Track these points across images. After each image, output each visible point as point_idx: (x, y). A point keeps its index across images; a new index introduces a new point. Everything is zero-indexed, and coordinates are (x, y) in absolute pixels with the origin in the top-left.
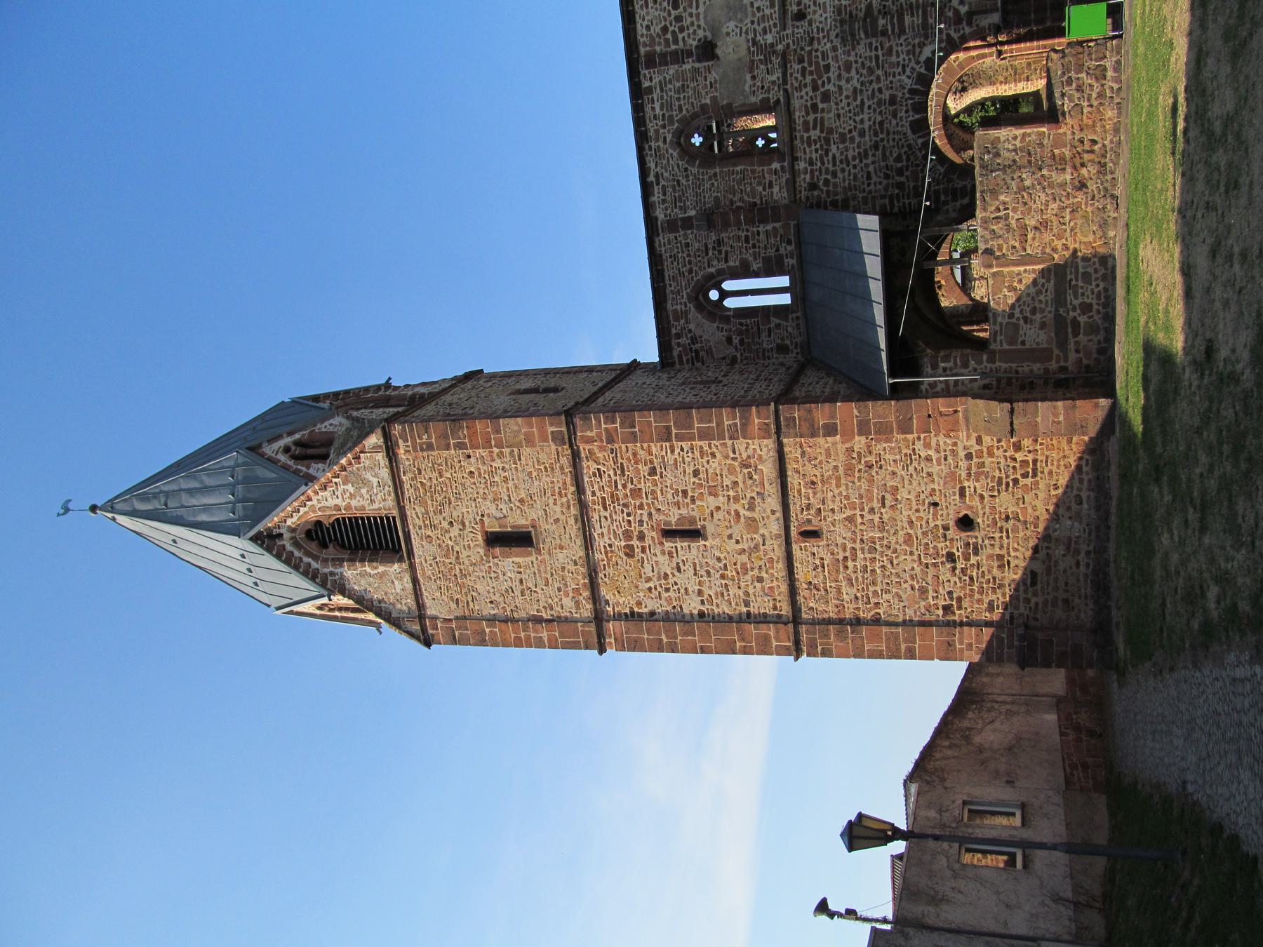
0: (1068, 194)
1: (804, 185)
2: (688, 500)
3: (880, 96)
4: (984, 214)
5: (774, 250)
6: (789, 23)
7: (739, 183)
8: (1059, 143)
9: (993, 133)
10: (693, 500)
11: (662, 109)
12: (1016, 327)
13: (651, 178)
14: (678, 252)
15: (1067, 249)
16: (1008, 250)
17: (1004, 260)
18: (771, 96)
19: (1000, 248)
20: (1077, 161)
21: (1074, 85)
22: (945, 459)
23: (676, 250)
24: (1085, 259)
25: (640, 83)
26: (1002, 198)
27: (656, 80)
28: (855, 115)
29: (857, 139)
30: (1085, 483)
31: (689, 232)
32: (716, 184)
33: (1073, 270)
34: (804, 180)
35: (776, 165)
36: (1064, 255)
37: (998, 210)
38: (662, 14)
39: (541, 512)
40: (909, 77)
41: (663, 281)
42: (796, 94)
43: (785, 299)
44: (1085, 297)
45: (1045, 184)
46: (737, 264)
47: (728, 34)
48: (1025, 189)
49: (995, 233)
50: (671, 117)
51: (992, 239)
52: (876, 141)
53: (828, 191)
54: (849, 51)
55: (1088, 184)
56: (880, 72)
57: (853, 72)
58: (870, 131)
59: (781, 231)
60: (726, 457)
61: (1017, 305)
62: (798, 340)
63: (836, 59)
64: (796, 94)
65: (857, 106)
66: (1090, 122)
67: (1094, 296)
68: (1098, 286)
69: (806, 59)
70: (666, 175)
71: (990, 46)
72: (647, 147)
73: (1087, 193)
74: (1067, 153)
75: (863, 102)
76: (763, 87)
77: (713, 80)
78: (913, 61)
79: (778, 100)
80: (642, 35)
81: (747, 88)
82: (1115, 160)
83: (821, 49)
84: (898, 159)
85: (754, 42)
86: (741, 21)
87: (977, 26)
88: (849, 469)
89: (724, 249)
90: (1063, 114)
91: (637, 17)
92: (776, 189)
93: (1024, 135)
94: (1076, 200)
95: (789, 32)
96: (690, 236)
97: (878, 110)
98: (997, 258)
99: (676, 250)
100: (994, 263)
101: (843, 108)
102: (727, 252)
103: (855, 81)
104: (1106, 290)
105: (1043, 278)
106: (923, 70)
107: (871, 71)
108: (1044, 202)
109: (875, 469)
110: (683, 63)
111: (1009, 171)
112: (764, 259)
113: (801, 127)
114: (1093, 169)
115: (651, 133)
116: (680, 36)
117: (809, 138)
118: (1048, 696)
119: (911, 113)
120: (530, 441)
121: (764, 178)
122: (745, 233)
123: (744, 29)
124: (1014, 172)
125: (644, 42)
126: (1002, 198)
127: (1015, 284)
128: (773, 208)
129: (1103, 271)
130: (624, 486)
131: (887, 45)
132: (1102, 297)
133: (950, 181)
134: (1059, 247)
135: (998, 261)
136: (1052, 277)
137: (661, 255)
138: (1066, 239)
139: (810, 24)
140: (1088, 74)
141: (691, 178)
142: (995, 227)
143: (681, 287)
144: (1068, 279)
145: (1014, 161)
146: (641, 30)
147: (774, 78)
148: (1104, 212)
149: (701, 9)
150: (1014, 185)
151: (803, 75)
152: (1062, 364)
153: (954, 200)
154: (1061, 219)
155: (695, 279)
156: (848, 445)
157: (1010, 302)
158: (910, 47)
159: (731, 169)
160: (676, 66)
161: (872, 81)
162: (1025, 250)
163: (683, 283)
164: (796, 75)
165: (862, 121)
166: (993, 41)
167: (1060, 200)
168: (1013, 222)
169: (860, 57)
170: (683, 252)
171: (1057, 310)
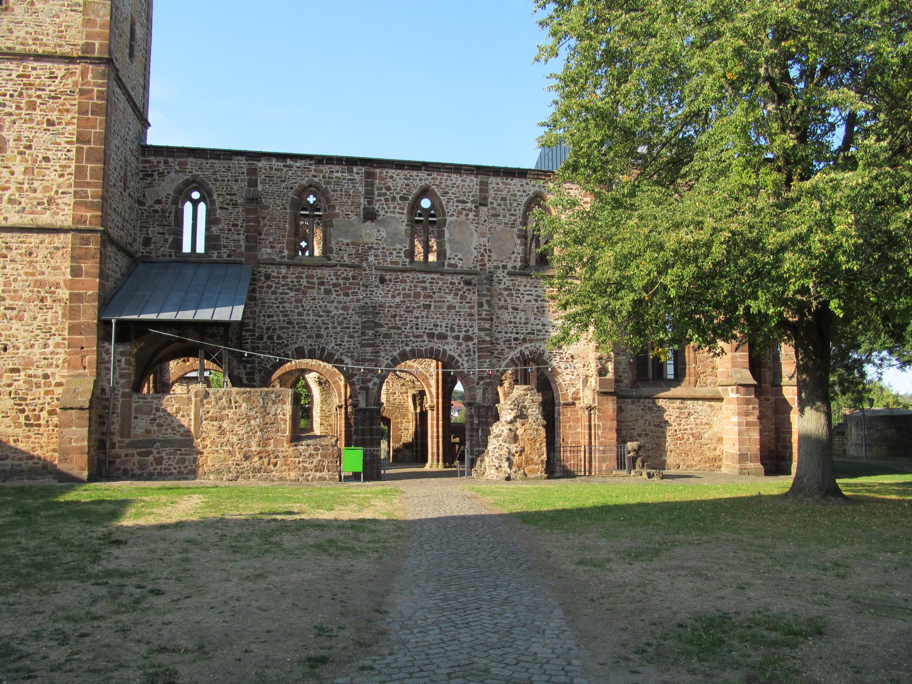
2: (22, 149)
6: (379, 273)
7: (277, 225)
8: (278, 442)
9: (289, 400)
10: (21, 153)
11: (336, 177)
12: (149, 413)
13: (289, 162)
19: (208, 403)
20: (264, 454)
22: (45, 359)
24: (195, 460)
25: (356, 165)
26: (244, 405)
27: (356, 177)
29: (296, 311)
30: (19, 462)
34: (273, 271)
35: (286, 252)
37: (236, 402)
39: (20, 18)
41: (211, 158)
43: (187, 248)
45: (251, 433)
47: (379, 231)
48: (249, 421)
50: (330, 183)
53: (263, 287)
56: (339, 329)
57: (342, 312)
59: (238, 251)
60: (59, 186)
62: (153, 255)
66: (289, 462)
68: (175, 468)
70: (290, 173)
71: (346, 401)
75: (321, 316)
79: (330, 260)
81: (342, 239)
84: (279, 337)
85: (370, 248)
86: (386, 241)
88: (41, 284)
89: (230, 207)
90: (296, 445)
92: (269, 251)
93: (285, 420)
95: (374, 272)
98: (202, 401)
102: (227, 209)
104: (171, 474)
106: (336, 357)
107: (340, 323)
109: (40, 304)
112: (219, 236)
115: (321, 167)
116: (382, 198)
117: (302, 278)
120: (87, 23)
124: (261, 413)
130: (39, 97)
133: (260, 371)
134: (205, 443)
139: (376, 286)
146: (391, 172)
147: (346, 258)
149: (397, 215)
150: (252, 413)
151: (344, 278)
152: (117, 445)
153: (247, 374)
156: (62, 284)
157: (169, 409)
165: (308, 315)
166: (348, 403)
168: (226, 412)
171: (159, 441)
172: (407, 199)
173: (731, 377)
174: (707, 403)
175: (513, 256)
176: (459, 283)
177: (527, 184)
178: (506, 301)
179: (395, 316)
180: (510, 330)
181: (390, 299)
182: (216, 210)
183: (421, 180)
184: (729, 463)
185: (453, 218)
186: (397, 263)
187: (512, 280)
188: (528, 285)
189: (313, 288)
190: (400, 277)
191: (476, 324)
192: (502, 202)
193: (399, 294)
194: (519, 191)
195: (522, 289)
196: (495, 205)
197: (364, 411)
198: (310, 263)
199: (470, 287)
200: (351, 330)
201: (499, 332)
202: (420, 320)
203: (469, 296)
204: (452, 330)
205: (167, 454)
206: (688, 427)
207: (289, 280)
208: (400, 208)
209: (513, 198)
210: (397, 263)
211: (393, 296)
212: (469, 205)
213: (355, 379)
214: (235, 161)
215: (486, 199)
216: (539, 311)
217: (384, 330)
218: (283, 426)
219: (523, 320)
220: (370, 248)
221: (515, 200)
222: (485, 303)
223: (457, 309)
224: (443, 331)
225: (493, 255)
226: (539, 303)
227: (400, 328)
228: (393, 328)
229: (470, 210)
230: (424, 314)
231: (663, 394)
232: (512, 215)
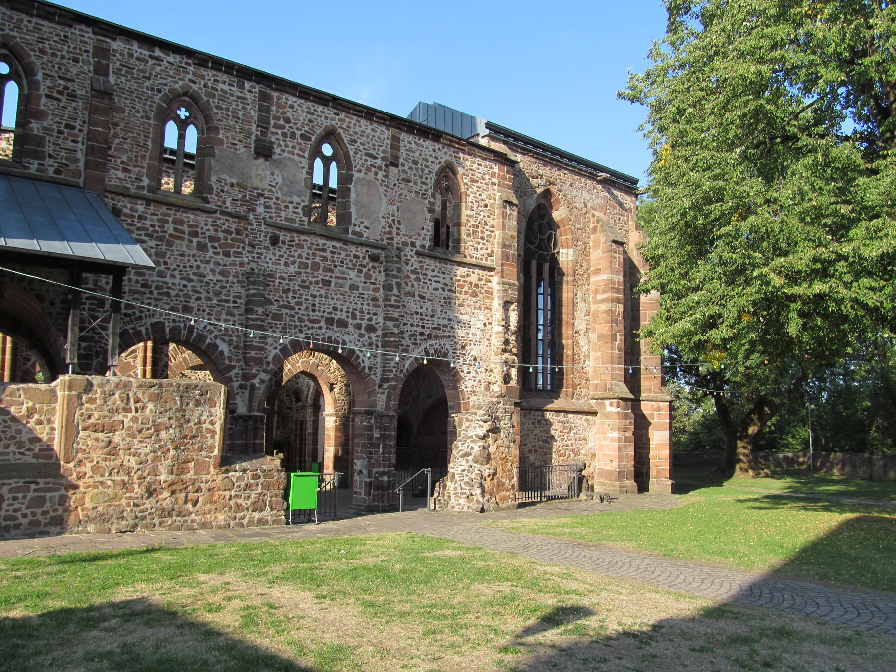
0: (145, 478)
1: (119, 205)
3: (193, 298)
4: (135, 385)
5: (51, 152)
6: (270, 230)
8: (201, 467)
9: (221, 400)
11: (222, 90)
13: (158, 53)
14: (69, 47)
15: (79, 478)
16: (87, 410)
17: (76, 404)
18: (213, 196)
19: (91, 401)
20: (178, 487)
21: (252, 481)
23: (72, 46)
24: (64, 499)
25: (250, 80)
26: (151, 406)
27: (248, 95)
28: (181, 271)
31: (91, 68)
32: (139, 115)
33: (50, 485)
35: (146, 182)
36: (71, 475)
37: (137, 401)
38: (300, 123)
40: (205, 327)
41: (38, 16)
42: (210, 220)
44: (11, 501)
45: (159, 453)
46: (42, 107)
47: (273, 174)
48: (158, 431)
49: (110, 395)
50: (213, 96)
51: (103, 392)
52: (151, 287)
54: (238, 277)
55: (151, 499)
56: (215, 301)
57: (219, 277)
58: (162, 282)
59: (72, 167)
61: (7, 418)
63: (234, 264)
64: (210, 220)
65: (188, 274)
66: (215, 498)
67: (11, 513)
68: (25, 516)
69: (238, 237)
70: (158, 68)
72: (190, 61)
73: (142, 498)
74: (189, 476)
75: (190, 280)
76: (222, 191)
77: (238, 147)
78: (218, 333)
79: (208, 202)
80: (287, 99)
81: (225, 176)
82: (174, 525)
83: (244, 252)
85: (261, 195)
86: (281, 189)
87: (238, 393)
90: (227, 471)
91: (303, 101)
92: (121, 174)
93: (214, 432)
94: (136, 486)
95: (263, 228)
96: (86, 67)
97: (181, 294)
98: (79, 397)
99: (72, 46)
100: (74, 392)
101: (189, 261)
102: (58, 100)
103: (211, 277)
104: (17, 526)
105: (41, 450)
106: (208, 341)
107: (217, 294)
108: (140, 451)
110: (258, 126)
111: (179, 414)
112: (43, 138)
113: (178, 216)
114: (168, 504)
115: (203, 71)
116: (280, 132)
117: (167, 222)
118: (301, 444)
119: (172, 324)
121: (135, 166)
122: (78, 127)
123: (273, 189)
124: (177, 419)
125: (281, 98)
126: (151, 406)
127: (36, 416)
128: (104, 165)
129: (43, 521)
131: (236, 312)
132: (8, 523)
134: (83, 469)
135: (75, 399)
136: (40, 461)
137: (71, 26)
138: (91, 477)
139: (266, 248)
140: (260, 494)
141: (150, 92)
142: (117, 396)
143: (25, 33)
144: (39, 480)
145: (188, 421)
146: (292, 99)
147: (228, 204)
148: (118, 518)
149: (296, 158)
150: (164, 419)
151: (225, 231)
154: (116, 470)
155: (32, 53)
157: (13, 410)
158: (230, 332)
159: (151, 136)
160: (256, 119)
161: (208, 293)
162: (84, 429)
163: (29, 38)
164: (227, 224)
165: (173, 276)
167: (139, 470)
168: (121, 417)
169: (231, 286)
170: (68, 52)
172: (309, 139)
173: (611, 389)
174: (585, 417)
175: (422, 233)
176: (364, 258)
177: (439, 149)
178: (412, 286)
179: (288, 290)
180: (416, 322)
181: (282, 267)
182: (40, 96)
183: (326, 118)
184: (603, 481)
185: (362, 175)
186: (293, 221)
187: (420, 262)
188: (436, 270)
189: (182, 239)
190: (296, 239)
191: (381, 311)
192: (413, 166)
193: (293, 263)
194: (431, 156)
195: (429, 273)
196: (406, 168)
197: (246, 418)
198: (171, 200)
199: (376, 265)
200: (231, 305)
201: (405, 324)
202: (317, 299)
203: (374, 275)
204: (354, 316)
205: (10, 491)
206: (569, 442)
207: (148, 222)
208: (300, 150)
209: (424, 163)
210: (293, 221)
211: (286, 265)
212: (379, 162)
213: (233, 373)
214: (78, 31)
215: (397, 158)
216: (445, 303)
217: (274, 308)
218: (210, 441)
219: (430, 312)
220: (261, 195)
221: (427, 166)
222: (394, 286)
223: (361, 291)
224: (344, 317)
225: (401, 227)
226: (446, 292)
227: (292, 308)
228: (284, 307)
229: (380, 168)
230: (322, 292)
231: (549, 406)
232: (423, 183)
